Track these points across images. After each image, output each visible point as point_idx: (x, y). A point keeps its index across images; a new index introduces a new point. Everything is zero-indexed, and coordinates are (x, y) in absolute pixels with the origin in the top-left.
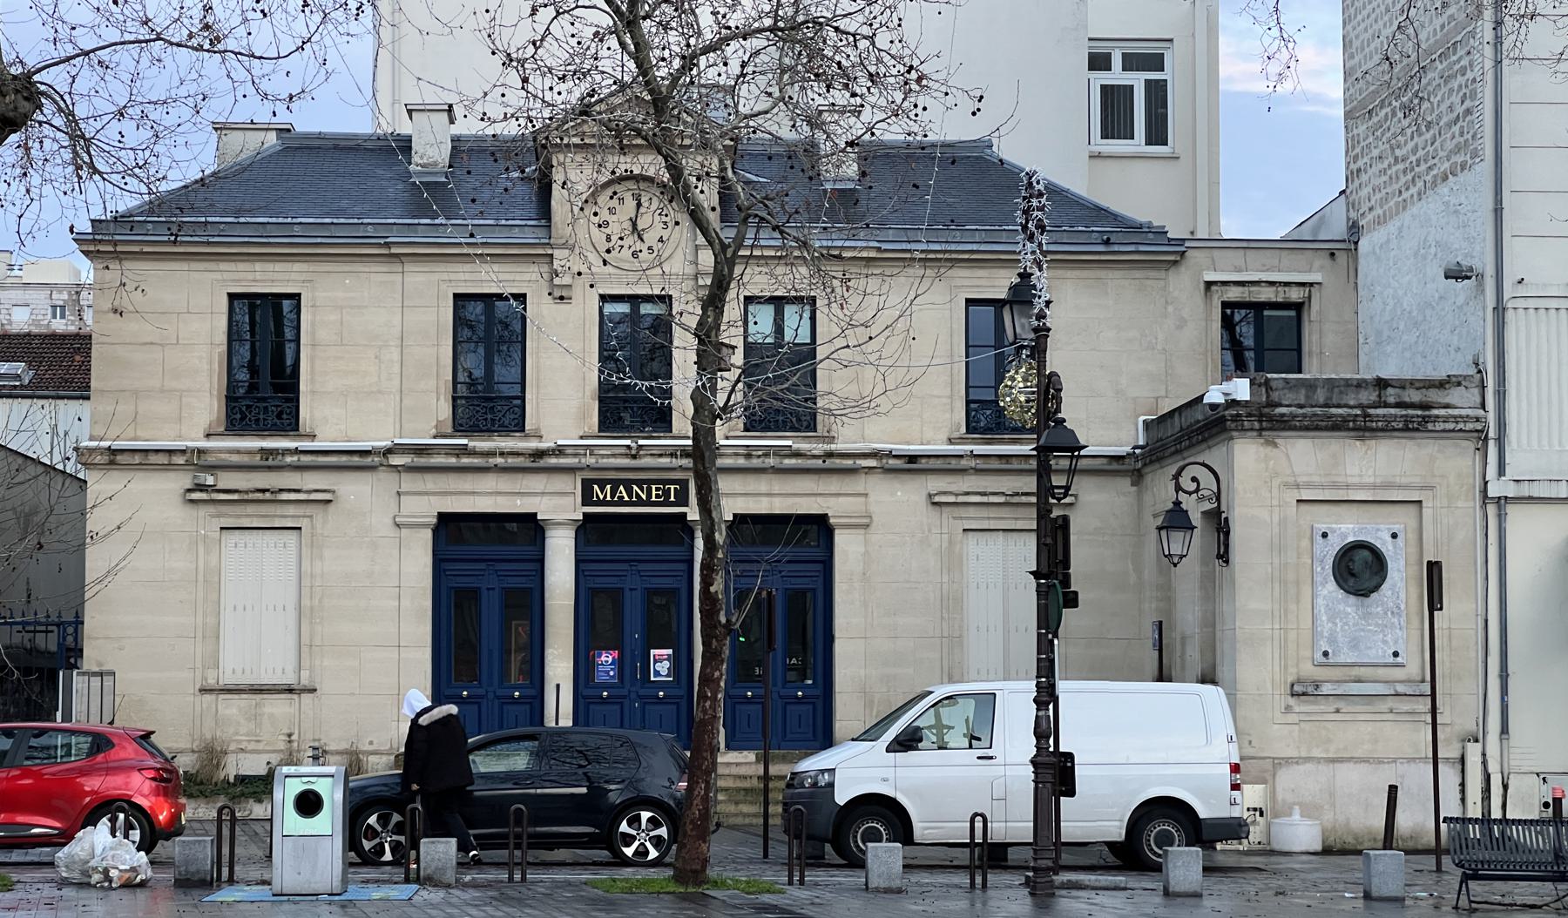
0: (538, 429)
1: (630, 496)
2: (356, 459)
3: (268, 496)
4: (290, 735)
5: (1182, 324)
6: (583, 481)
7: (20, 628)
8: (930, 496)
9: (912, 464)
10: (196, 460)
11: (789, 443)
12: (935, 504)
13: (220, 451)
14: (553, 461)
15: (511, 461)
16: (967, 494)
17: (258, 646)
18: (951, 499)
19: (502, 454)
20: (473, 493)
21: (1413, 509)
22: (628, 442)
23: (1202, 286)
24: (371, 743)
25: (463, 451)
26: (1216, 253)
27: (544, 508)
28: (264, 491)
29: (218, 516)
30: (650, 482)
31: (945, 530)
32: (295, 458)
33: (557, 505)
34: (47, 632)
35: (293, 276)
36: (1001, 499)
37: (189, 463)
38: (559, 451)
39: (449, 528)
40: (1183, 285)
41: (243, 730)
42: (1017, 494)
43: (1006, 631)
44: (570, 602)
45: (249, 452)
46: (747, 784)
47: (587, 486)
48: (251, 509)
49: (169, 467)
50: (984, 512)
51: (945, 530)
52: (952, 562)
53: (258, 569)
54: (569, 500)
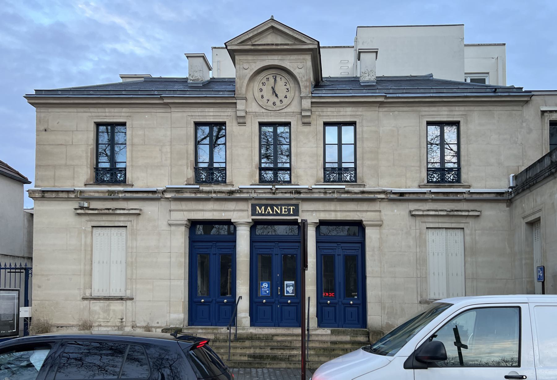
0: (232, 182)
1: (273, 212)
2: (150, 195)
3: (111, 211)
4: (122, 319)
5: (530, 131)
6: (252, 205)
7: (9, 270)
8: (410, 212)
9: (401, 197)
10: (80, 196)
11: (344, 187)
12: (413, 215)
13: (90, 192)
14: (238, 195)
15: (219, 195)
16: (428, 210)
17: (109, 277)
18: (421, 213)
19: (215, 192)
20: (203, 210)
21: (462, 230)
22: (271, 187)
23: (540, 113)
24: (158, 323)
25: (197, 191)
26: (547, 97)
27: (234, 217)
28: (109, 209)
29: (90, 221)
30: (281, 205)
31: (417, 228)
32: (123, 195)
33: (240, 215)
34: (20, 272)
35: (123, 114)
36: (445, 213)
37: (76, 197)
38: (241, 191)
39: (193, 224)
40: (530, 113)
41: (101, 316)
42: (452, 211)
43: (448, 275)
44: (248, 259)
45: (102, 192)
46: (325, 346)
47: (254, 207)
48: (104, 218)
49: (68, 199)
50: (436, 219)
51: (417, 228)
52: (421, 242)
53: (110, 245)
54: (245, 214)
